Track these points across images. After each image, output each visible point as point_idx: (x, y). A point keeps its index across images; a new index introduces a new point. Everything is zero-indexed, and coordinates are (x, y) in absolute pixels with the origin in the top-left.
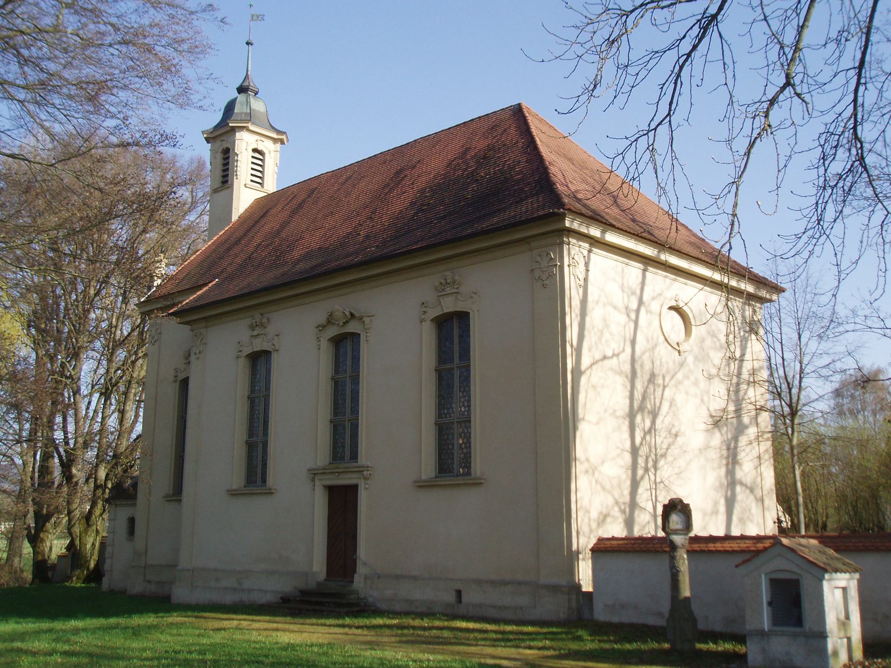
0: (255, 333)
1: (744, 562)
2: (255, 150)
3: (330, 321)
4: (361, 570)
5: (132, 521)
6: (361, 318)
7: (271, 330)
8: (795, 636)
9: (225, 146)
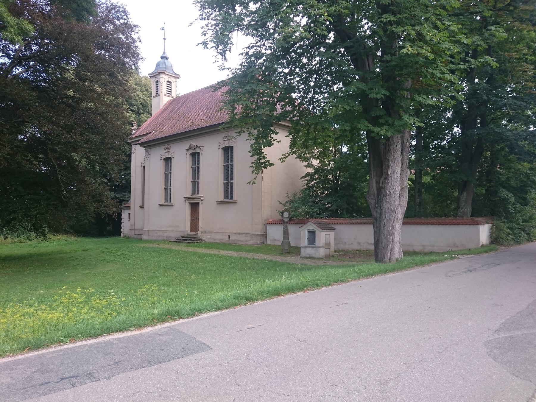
0: (166, 151)
1: (301, 227)
2: (168, 81)
3: (190, 148)
4: (200, 229)
5: (129, 214)
6: (200, 147)
7: (171, 151)
8: (313, 247)
9: (157, 80)
